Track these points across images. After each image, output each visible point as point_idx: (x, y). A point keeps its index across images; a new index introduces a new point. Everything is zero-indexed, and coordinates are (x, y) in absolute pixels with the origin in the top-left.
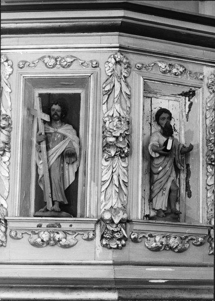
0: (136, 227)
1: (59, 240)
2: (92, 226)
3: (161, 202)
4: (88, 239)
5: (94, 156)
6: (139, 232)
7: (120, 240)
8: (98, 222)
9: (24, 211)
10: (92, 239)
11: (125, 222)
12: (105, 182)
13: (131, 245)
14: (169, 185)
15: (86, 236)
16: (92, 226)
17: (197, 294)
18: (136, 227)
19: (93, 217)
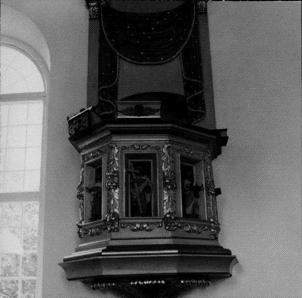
0: (181, 221)
1: (146, 227)
2: (161, 220)
3: (189, 210)
4: (159, 227)
5: (160, 188)
6: (183, 223)
7: (174, 226)
8: (163, 219)
9: (127, 215)
10: (161, 227)
11: (176, 218)
12: (165, 200)
13: (179, 230)
14: (193, 202)
15: (158, 225)
16: (161, 220)
17: (119, 268)
18: (181, 221)
19: (119, 103)
